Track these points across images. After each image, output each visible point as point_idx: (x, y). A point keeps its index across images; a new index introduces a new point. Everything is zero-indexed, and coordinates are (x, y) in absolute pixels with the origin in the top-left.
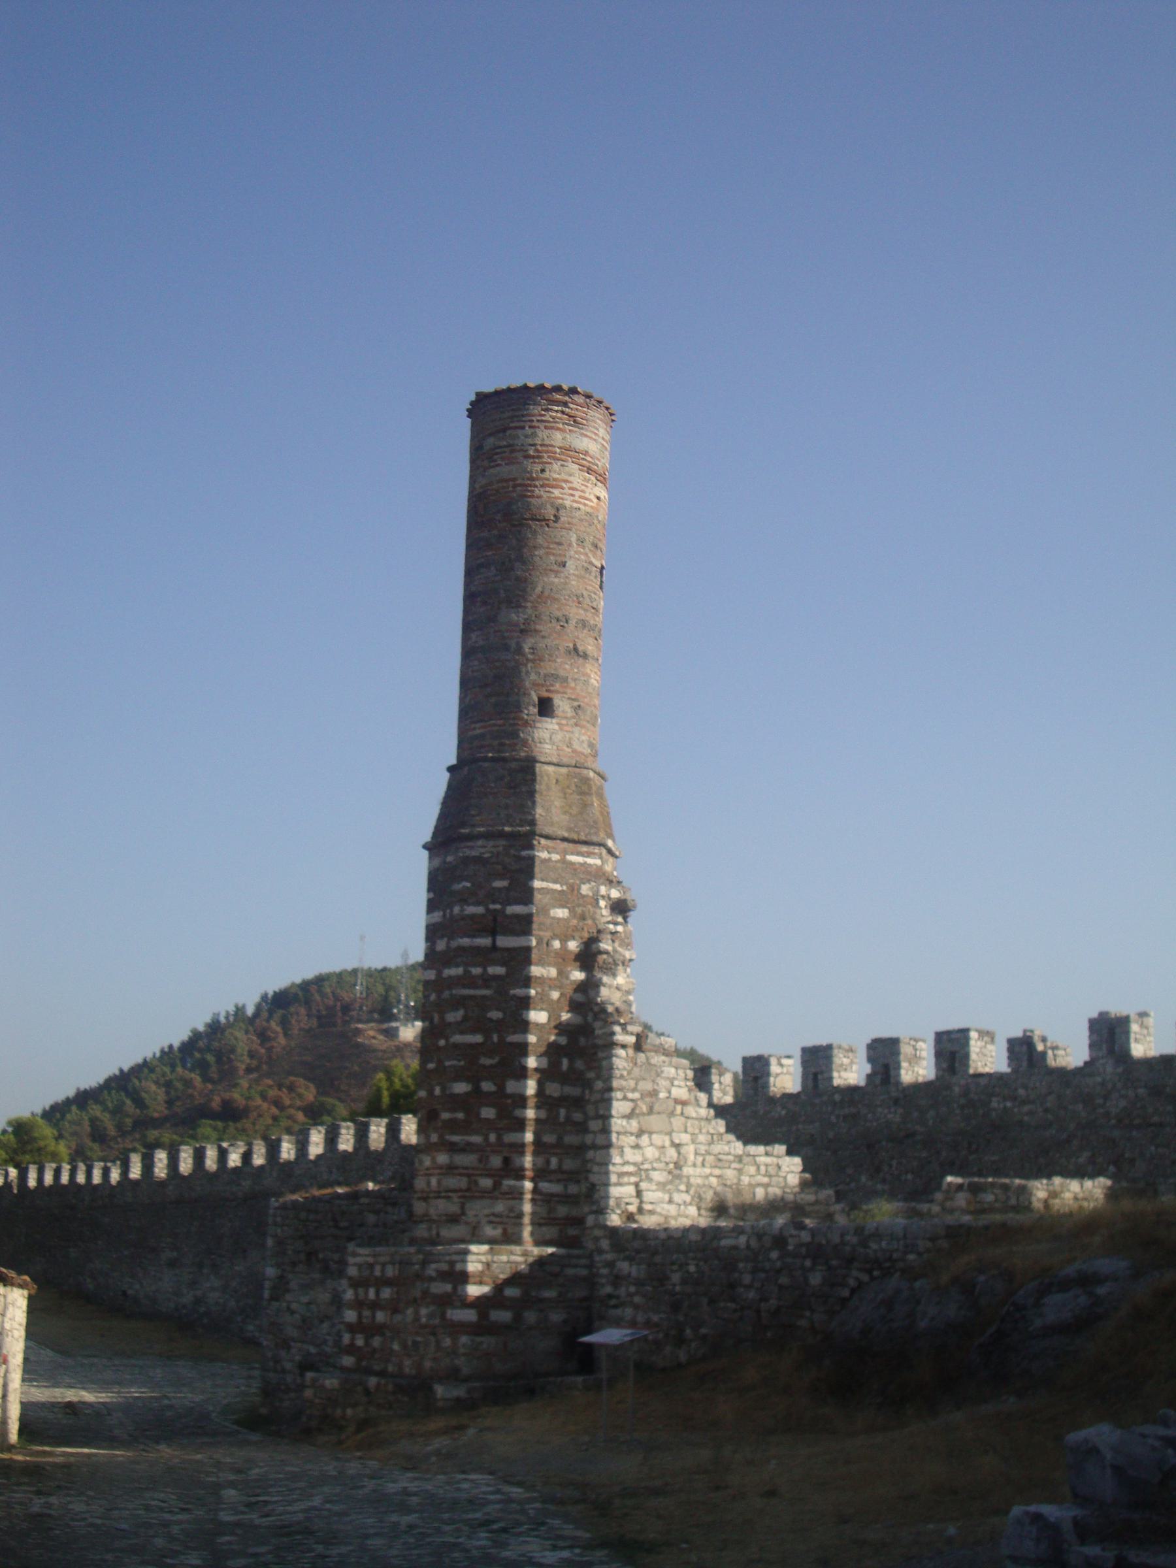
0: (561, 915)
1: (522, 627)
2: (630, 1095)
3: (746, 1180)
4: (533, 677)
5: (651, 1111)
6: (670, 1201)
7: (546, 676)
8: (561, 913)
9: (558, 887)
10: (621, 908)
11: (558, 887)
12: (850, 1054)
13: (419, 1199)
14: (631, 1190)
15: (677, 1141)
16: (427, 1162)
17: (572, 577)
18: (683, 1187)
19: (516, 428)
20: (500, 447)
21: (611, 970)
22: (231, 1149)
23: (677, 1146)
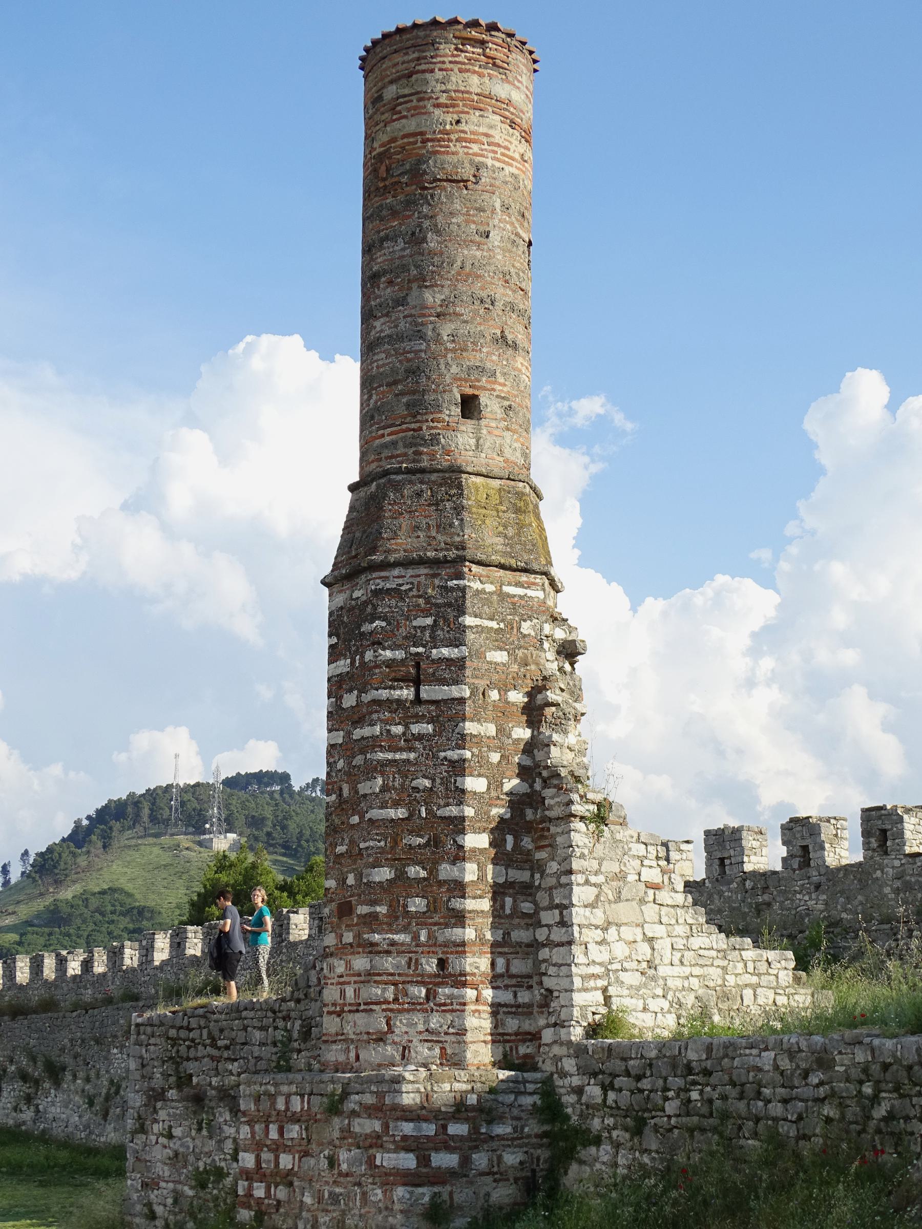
0: (499, 660)
1: (439, 310)
2: (593, 879)
3: (731, 980)
4: (454, 369)
5: (618, 899)
6: (645, 1009)
7: (469, 368)
8: (500, 657)
9: (494, 625)
10: (570, 652)
11: (494, 625)
12: (759, 837)
13: (329, 1013)
14: (599, 997)
15: (650, 935)
16: (340, 969)
17: (498, 251)
18: (659, 992)
19: (424, 71)
20: (405, 96)
21: (559, 725)
22: (70, 957)
23: (650, 940)
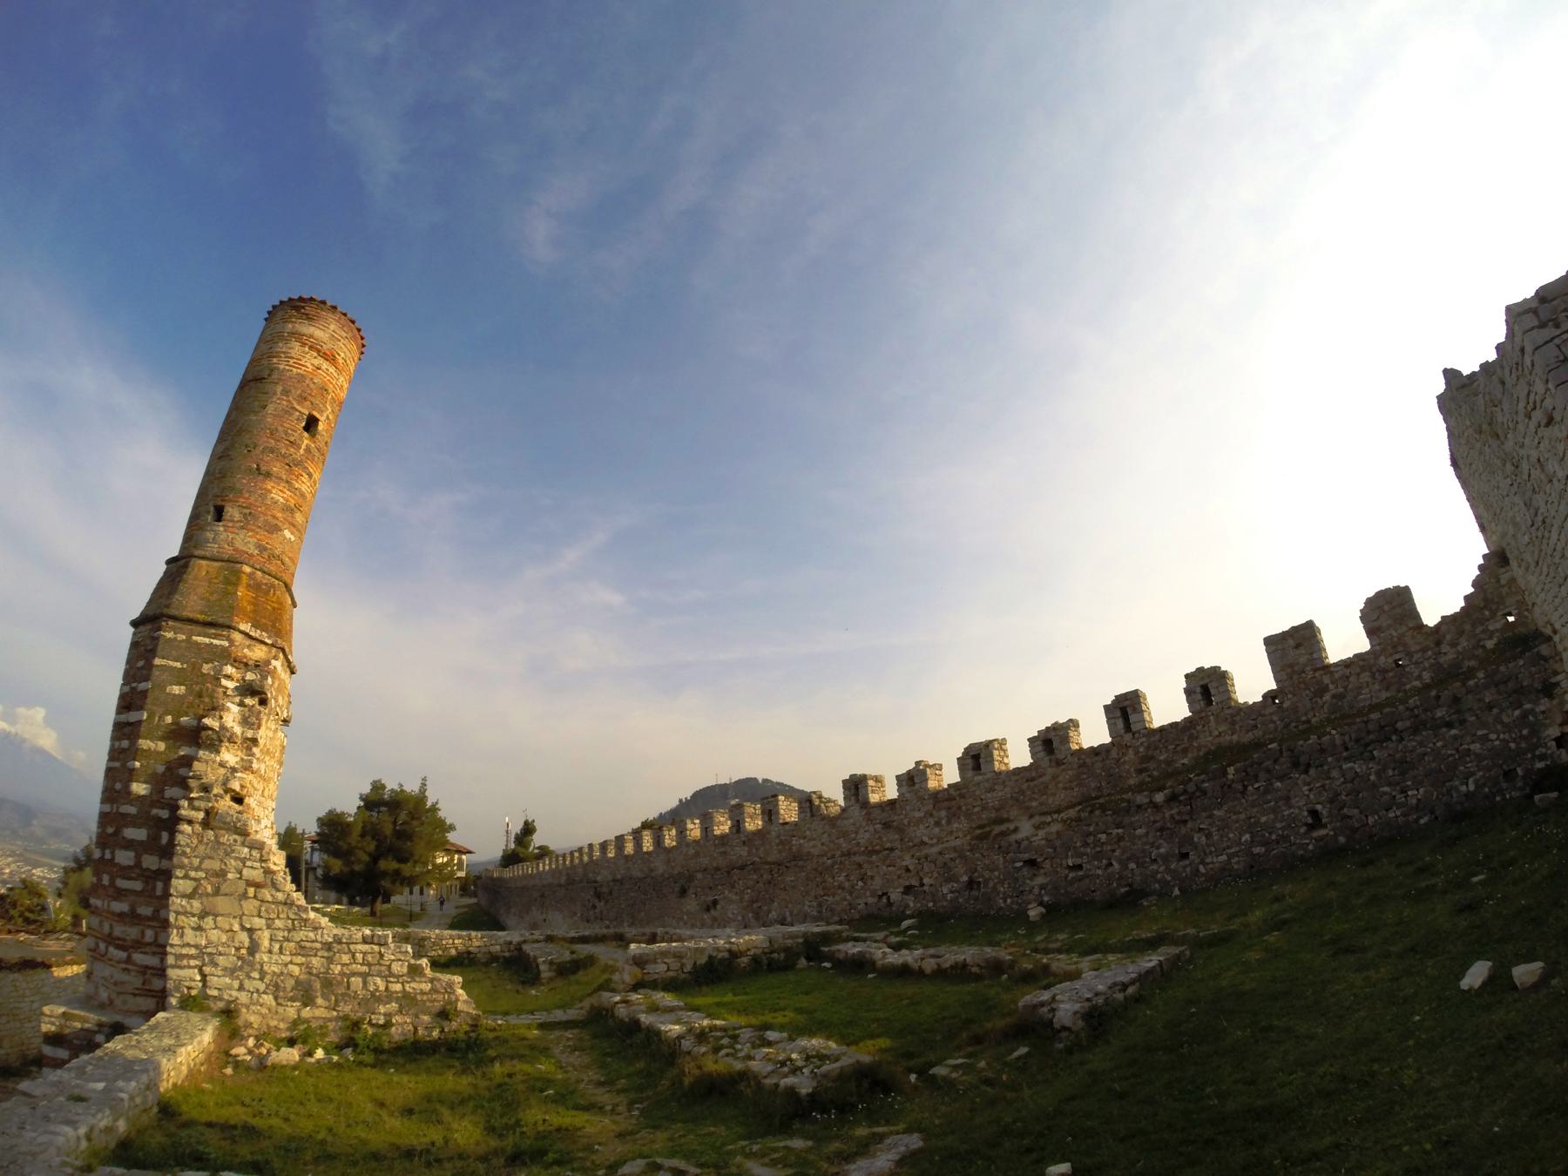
2: (193, 874)
5: (217, 892)
6: (241, 988)
8: (177, 690)
9: (178, 665)
11: (178, 665)
18: (256, 975)
23: (251, 931)
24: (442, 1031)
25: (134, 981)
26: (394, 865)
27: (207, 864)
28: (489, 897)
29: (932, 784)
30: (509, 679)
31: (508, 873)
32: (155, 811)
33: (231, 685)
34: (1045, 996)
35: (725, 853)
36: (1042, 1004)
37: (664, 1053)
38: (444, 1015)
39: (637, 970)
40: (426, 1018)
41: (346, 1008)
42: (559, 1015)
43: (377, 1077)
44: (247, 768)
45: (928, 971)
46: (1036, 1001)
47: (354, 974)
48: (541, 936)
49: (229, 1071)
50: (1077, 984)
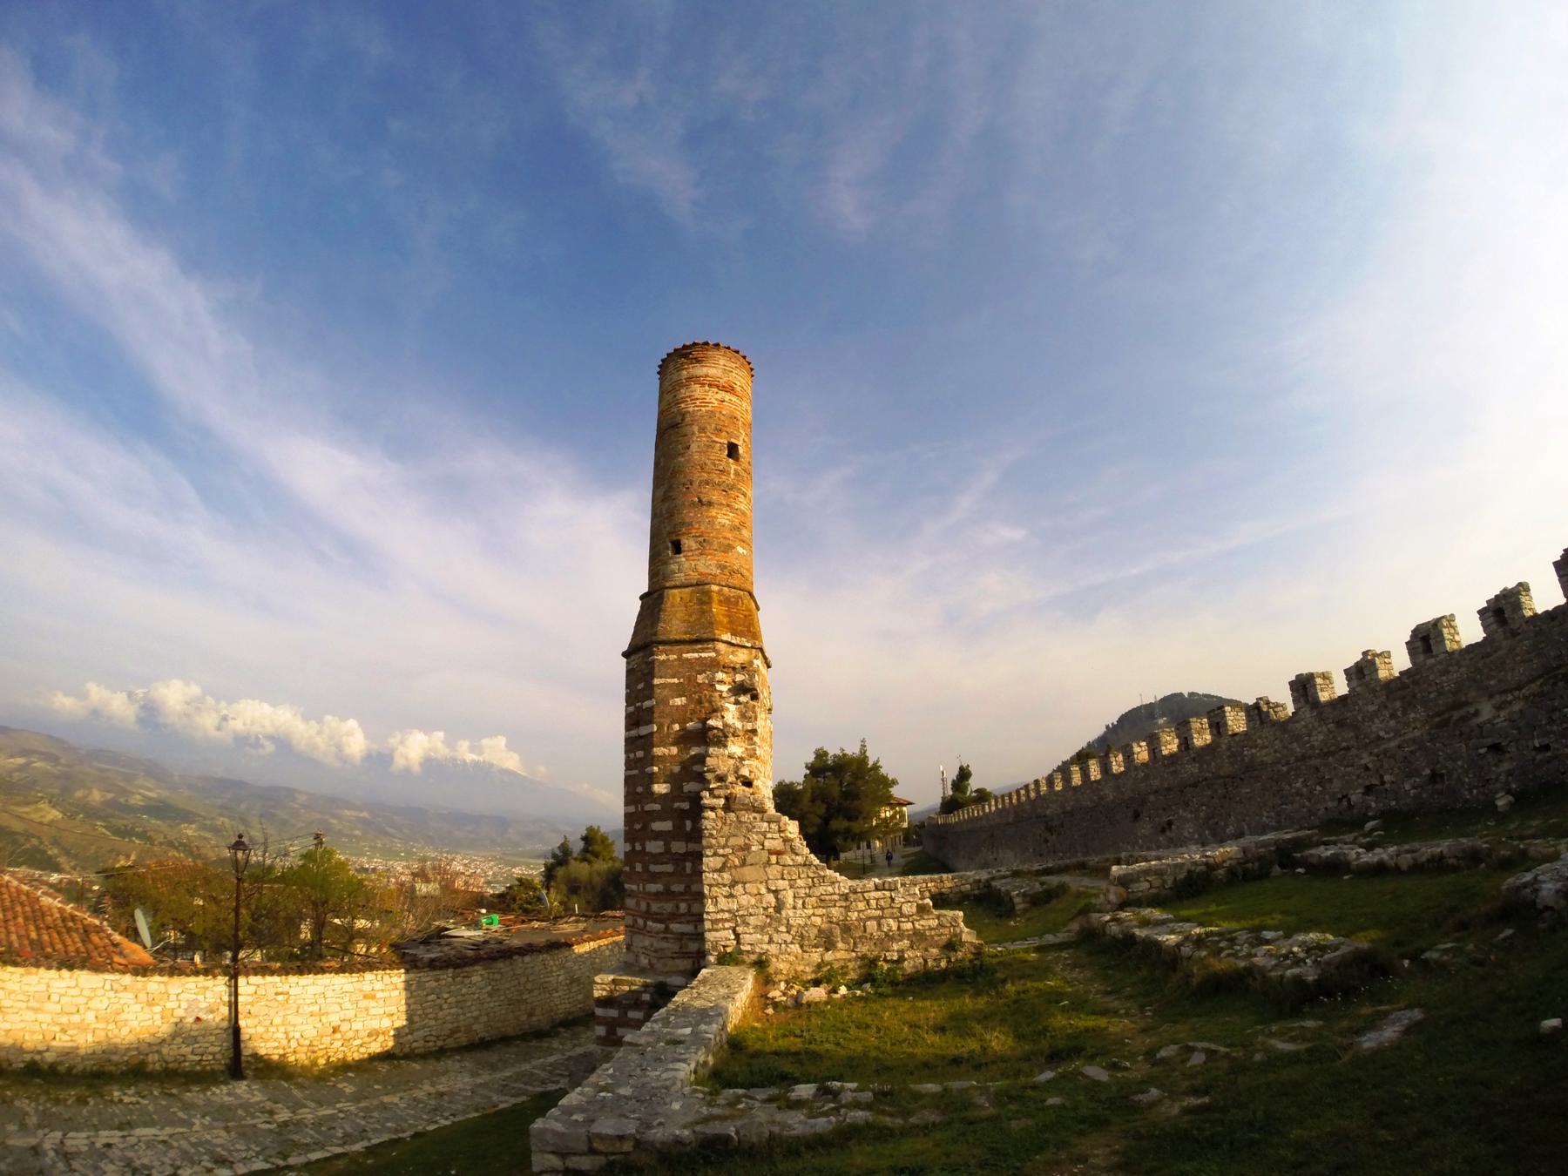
2: (721, 851)
5: (744, 863)
6: (771, 941)
8: (679, 701)
18: (783, 929)
23: (776, 892)
24: (949, 961)
25: (671, 946)
26: (845, 824)
27: (732, 841)
28: (938, 843)
29: (1383, 674)
30: (956, 641)
31: (953, 819)
32: (677, 805)
33: (724, 688)
34: (1528, 877)
35: (1175, 772)
36: (1525, 885)
37: (1169, 960)
38: (950, 946)
39: (1122, 890)
40: (934, 951)
41: (863, 949)
42: (1050, 938)
43: (904, 1006)
44: (753, 755)
45: (1404, 865)
46: (1518, 882)
47: (870, 918)
48: (1007, 871)
49: (770, 1011)
50: (1557, 865)
